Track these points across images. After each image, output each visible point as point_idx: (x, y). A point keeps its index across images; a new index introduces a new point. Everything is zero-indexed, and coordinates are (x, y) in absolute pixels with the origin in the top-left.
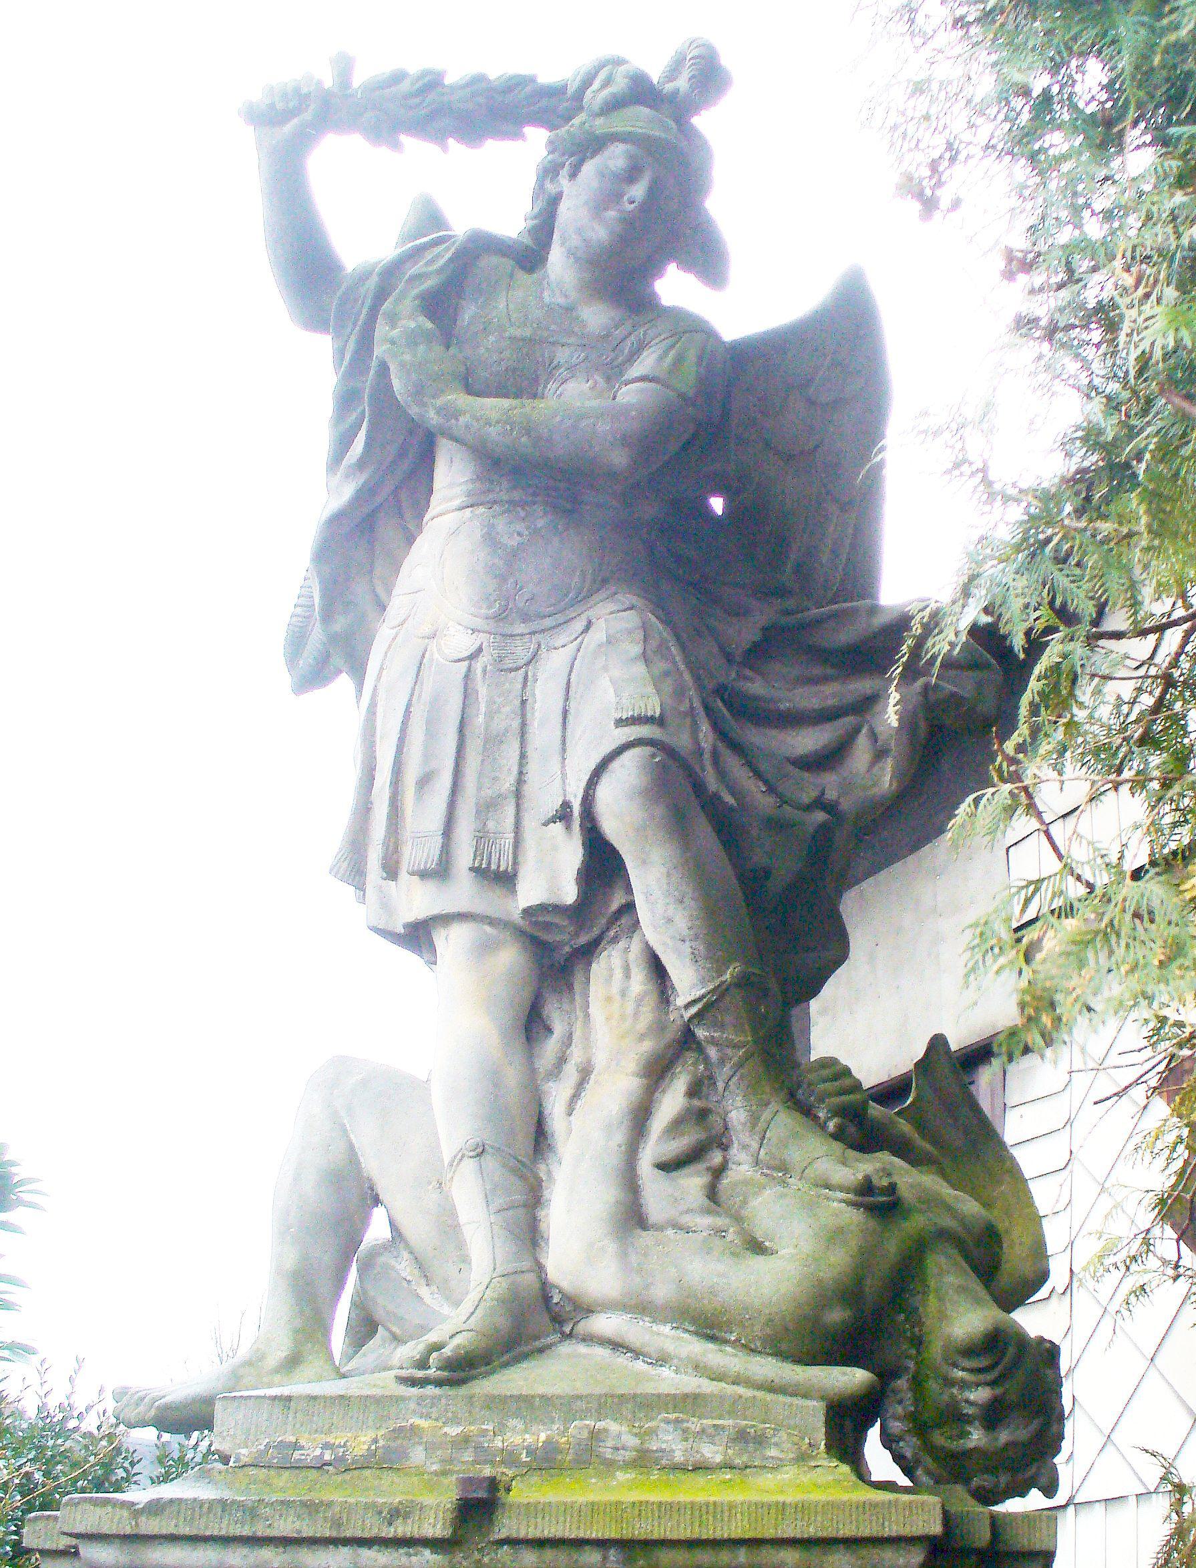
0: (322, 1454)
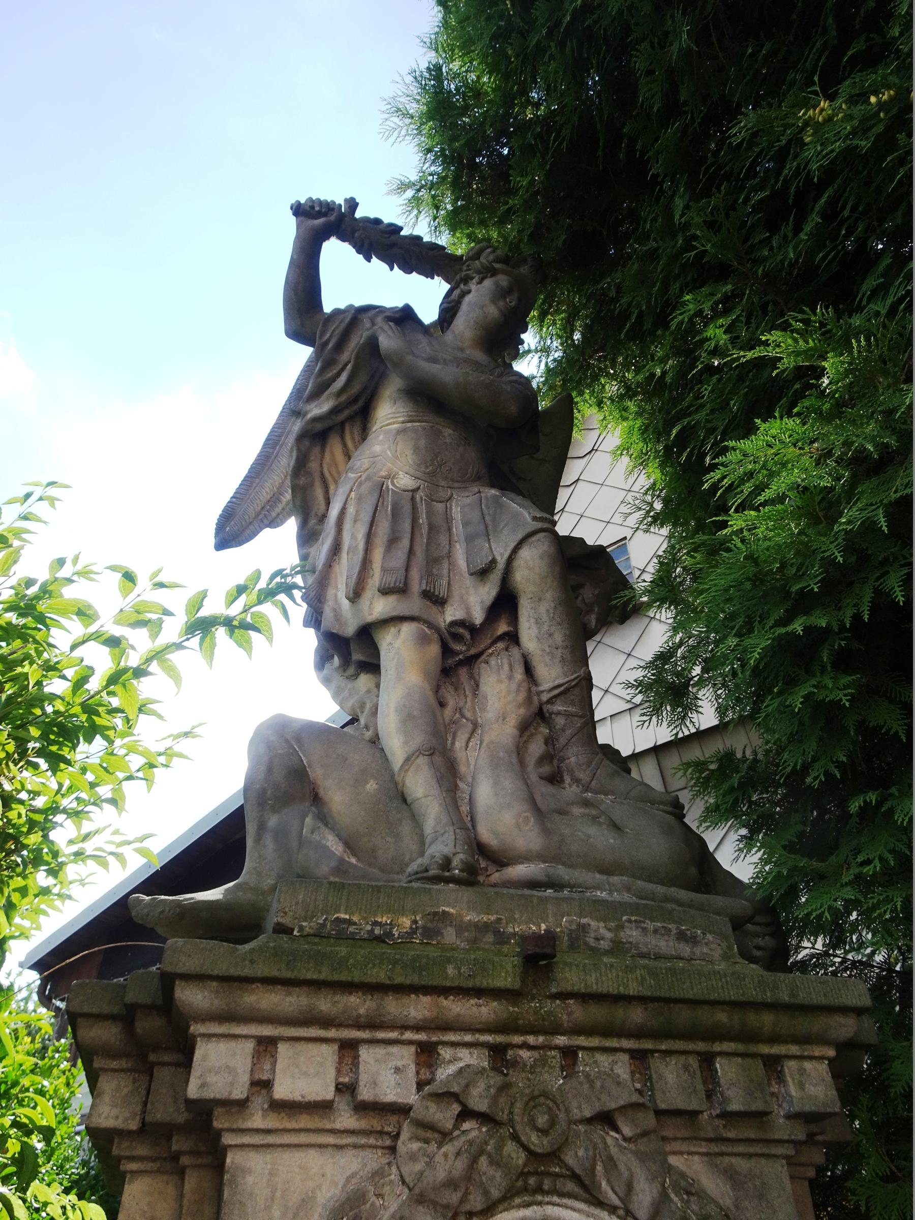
0: (372, 930)
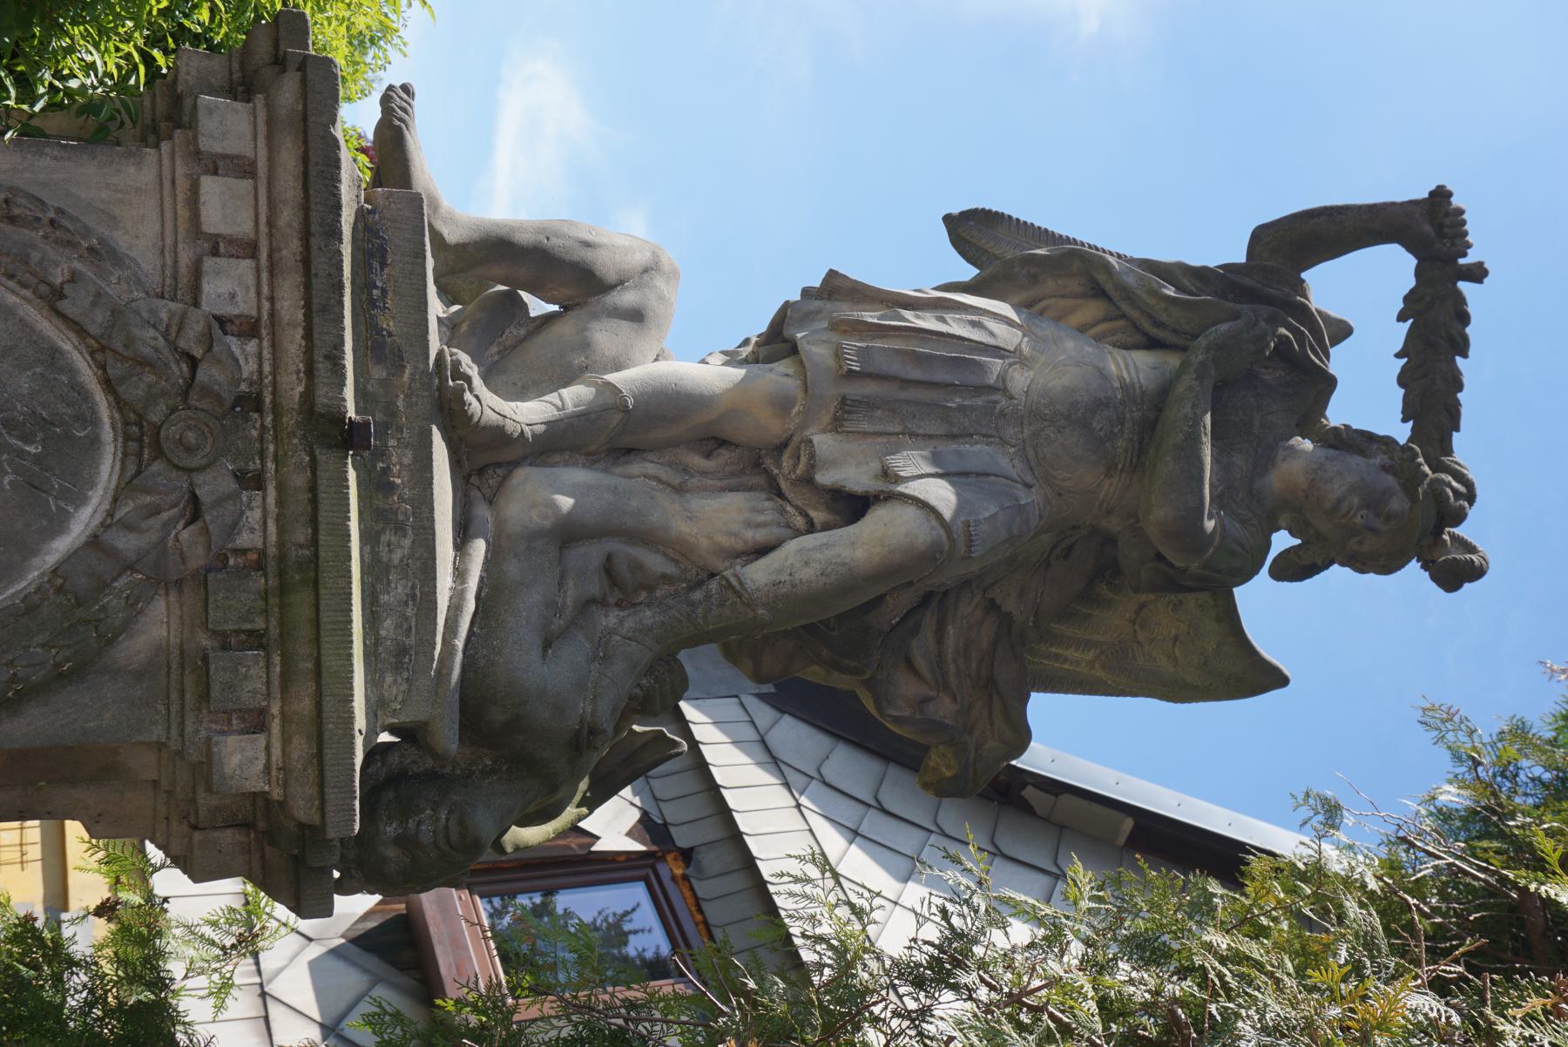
0: (376, 287)
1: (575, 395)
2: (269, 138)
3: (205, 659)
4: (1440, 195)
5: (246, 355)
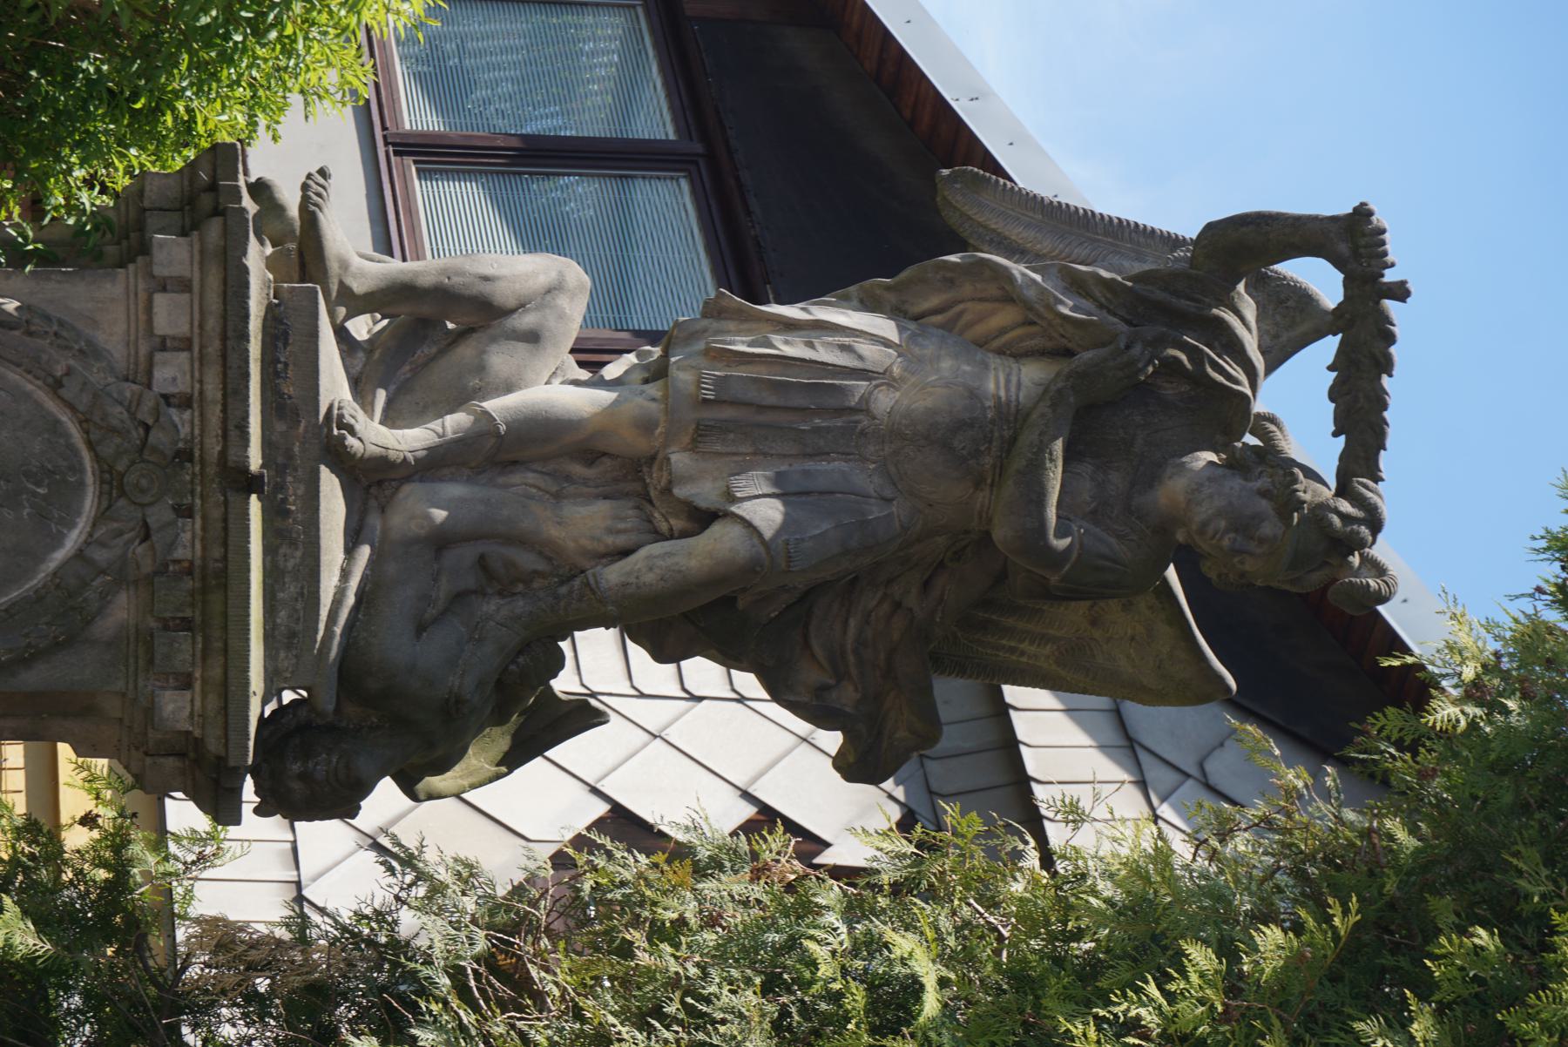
1: (455, 422)
2: (202, 263)
3: (152, 635)
4: (1362, 213)
5: (182, 419)
